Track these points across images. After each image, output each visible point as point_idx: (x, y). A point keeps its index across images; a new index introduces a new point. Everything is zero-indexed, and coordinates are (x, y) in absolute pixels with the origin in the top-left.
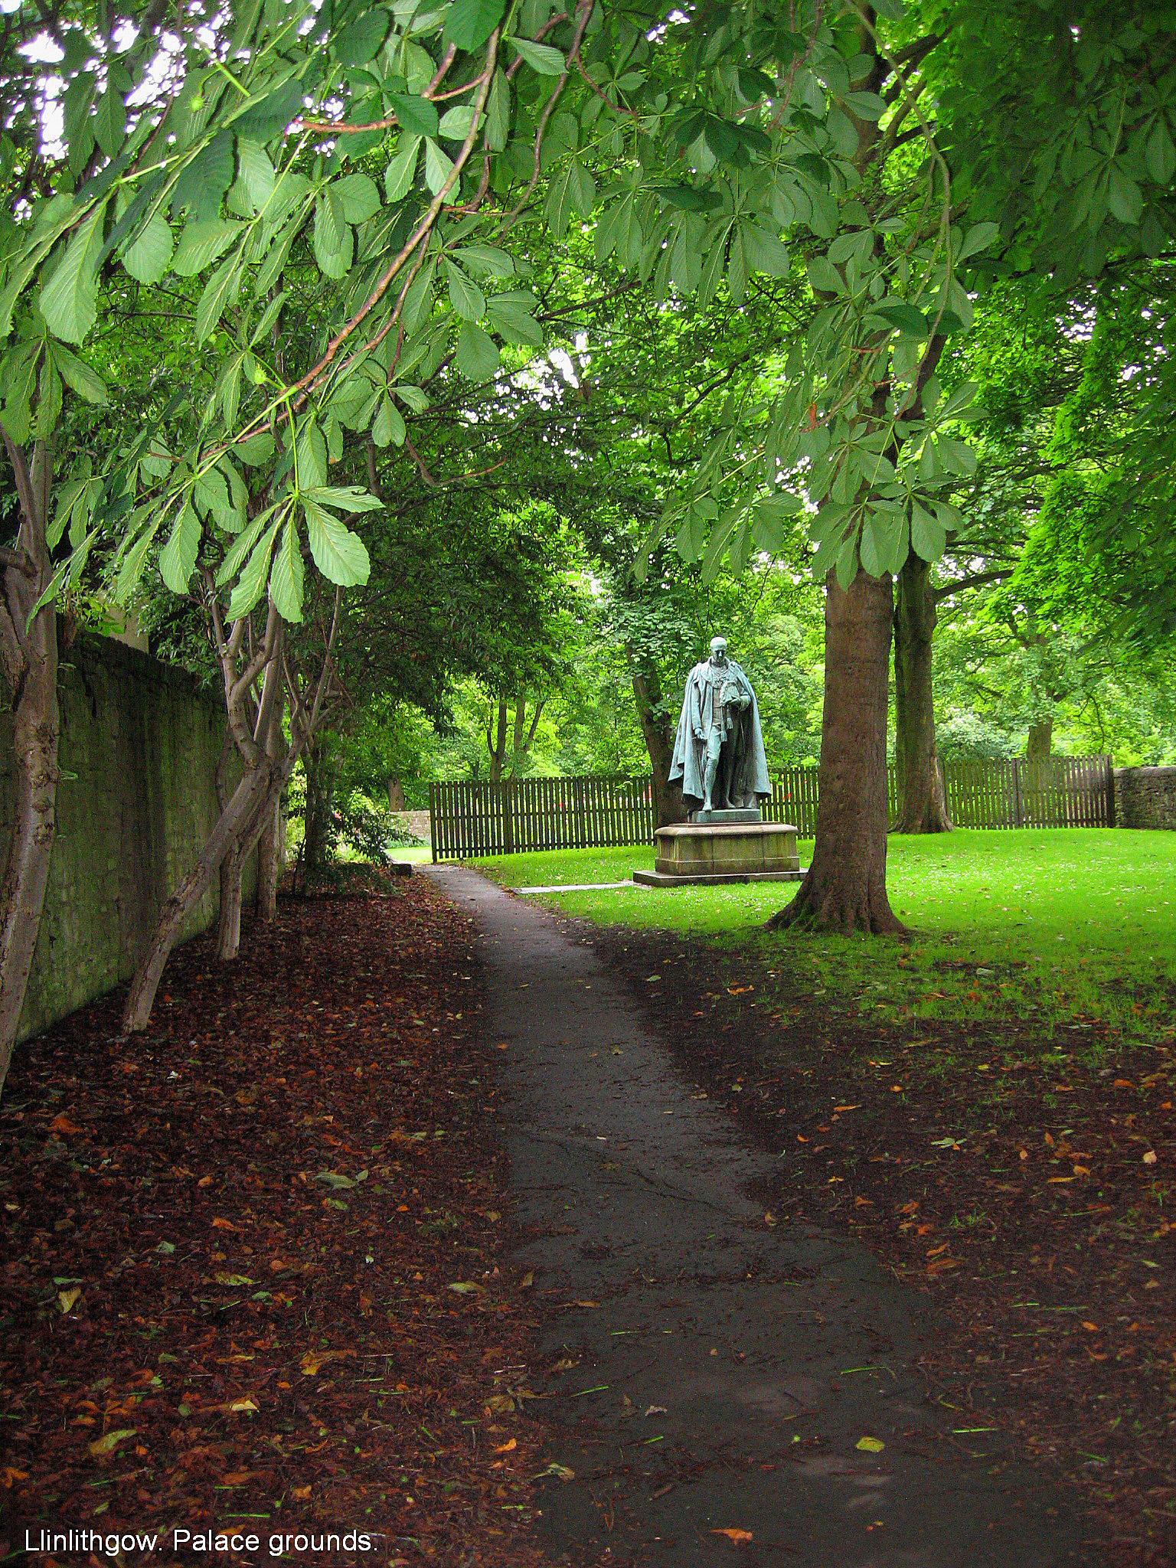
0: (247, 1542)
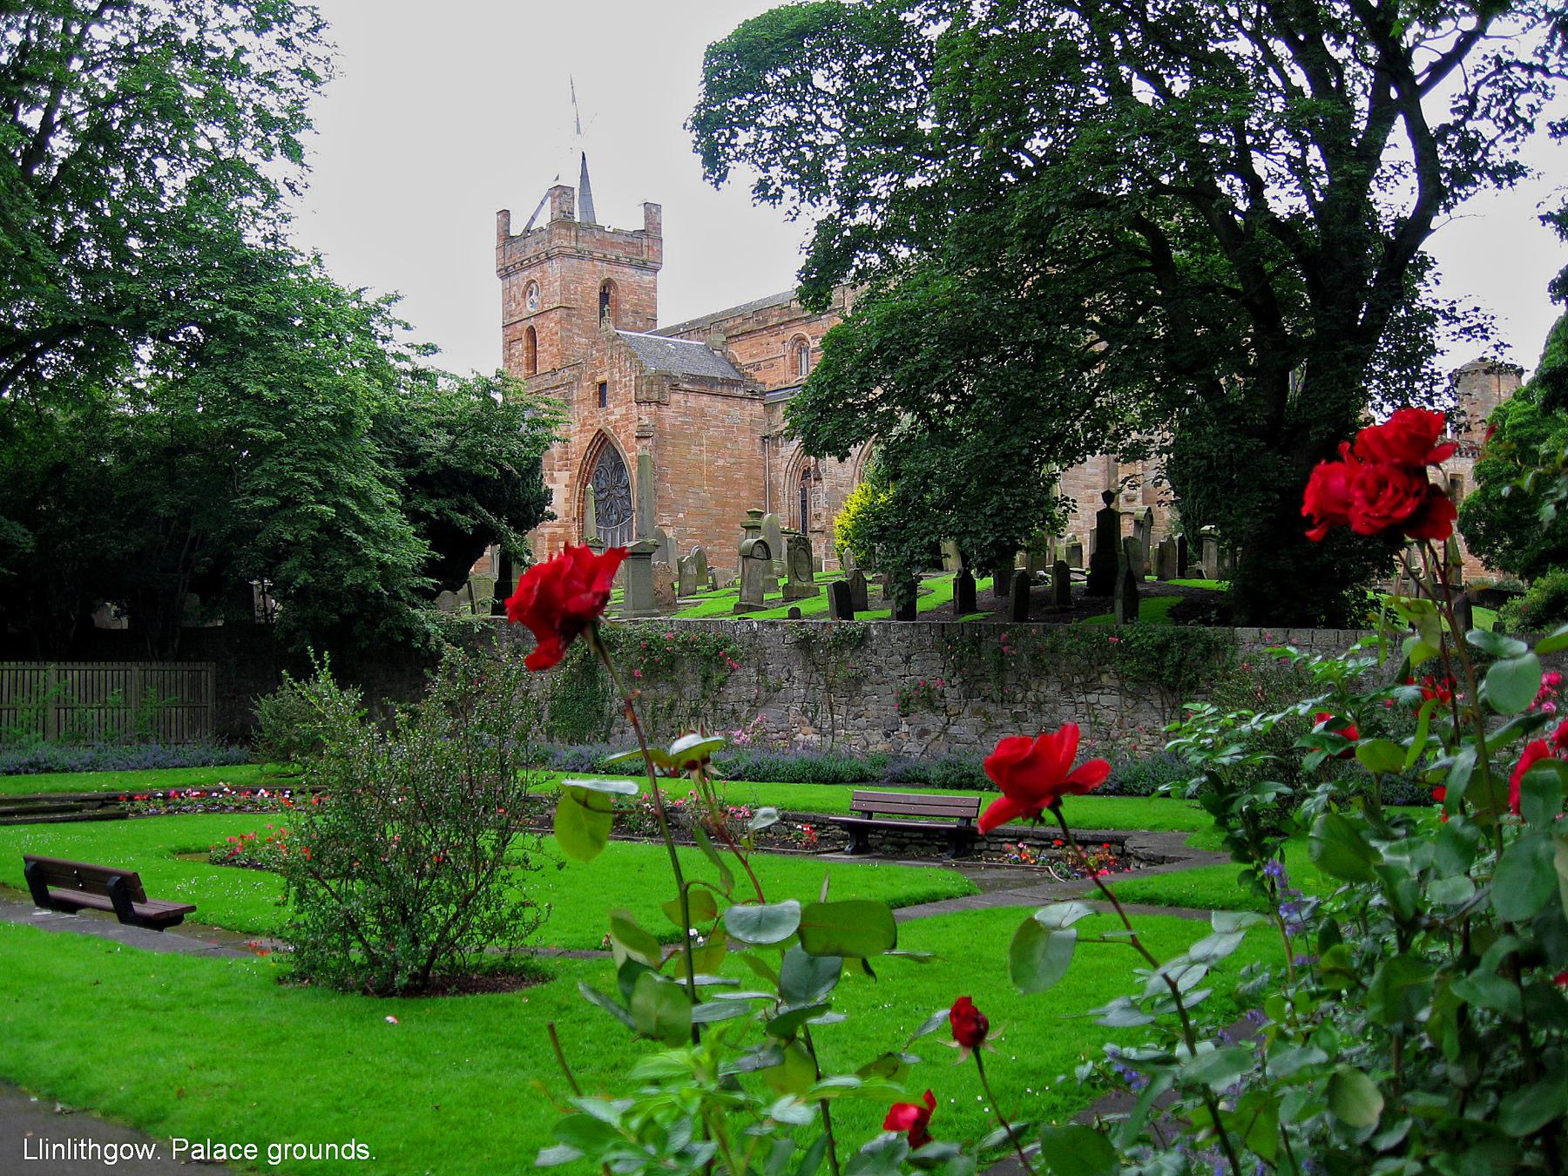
0: (246, 1151)
